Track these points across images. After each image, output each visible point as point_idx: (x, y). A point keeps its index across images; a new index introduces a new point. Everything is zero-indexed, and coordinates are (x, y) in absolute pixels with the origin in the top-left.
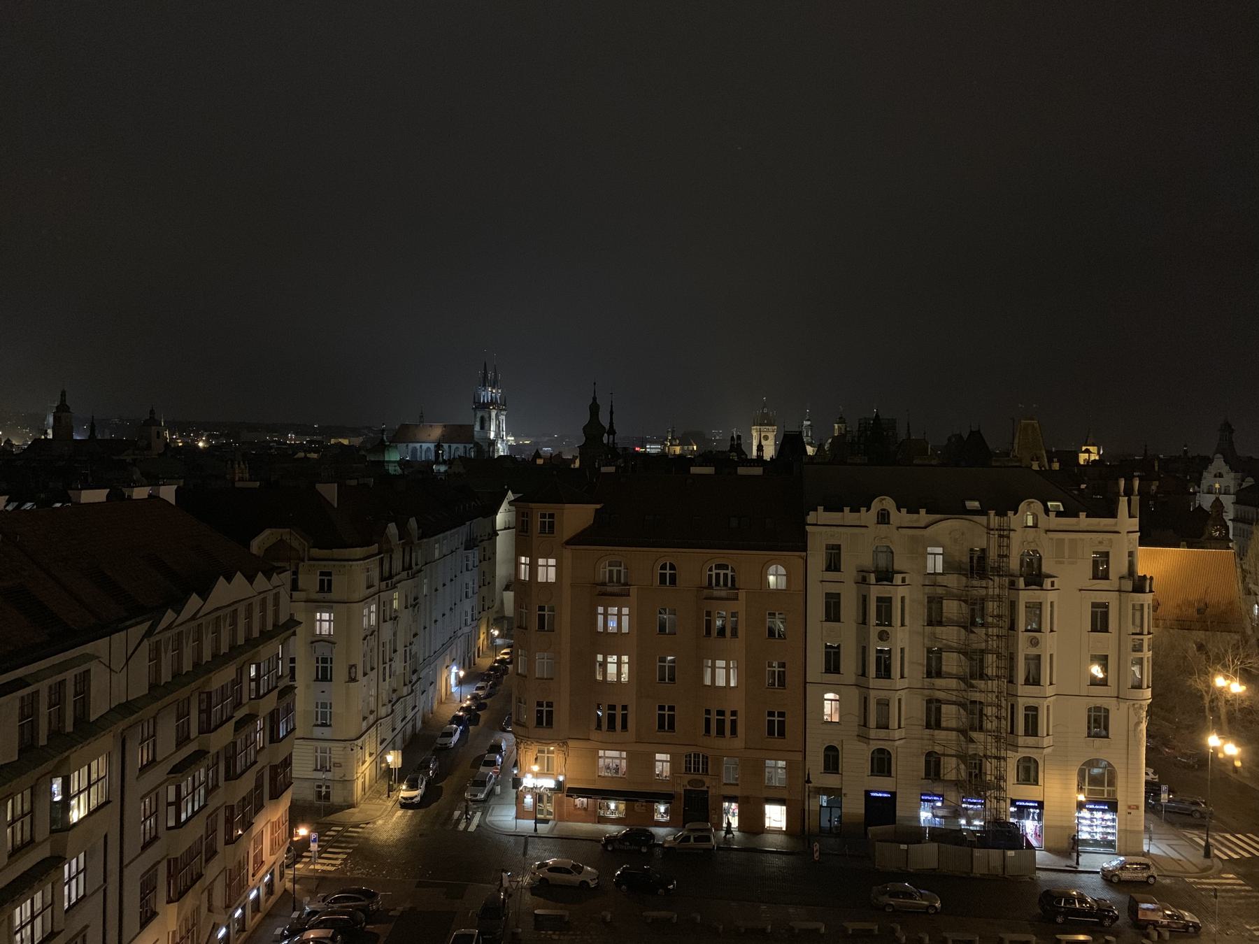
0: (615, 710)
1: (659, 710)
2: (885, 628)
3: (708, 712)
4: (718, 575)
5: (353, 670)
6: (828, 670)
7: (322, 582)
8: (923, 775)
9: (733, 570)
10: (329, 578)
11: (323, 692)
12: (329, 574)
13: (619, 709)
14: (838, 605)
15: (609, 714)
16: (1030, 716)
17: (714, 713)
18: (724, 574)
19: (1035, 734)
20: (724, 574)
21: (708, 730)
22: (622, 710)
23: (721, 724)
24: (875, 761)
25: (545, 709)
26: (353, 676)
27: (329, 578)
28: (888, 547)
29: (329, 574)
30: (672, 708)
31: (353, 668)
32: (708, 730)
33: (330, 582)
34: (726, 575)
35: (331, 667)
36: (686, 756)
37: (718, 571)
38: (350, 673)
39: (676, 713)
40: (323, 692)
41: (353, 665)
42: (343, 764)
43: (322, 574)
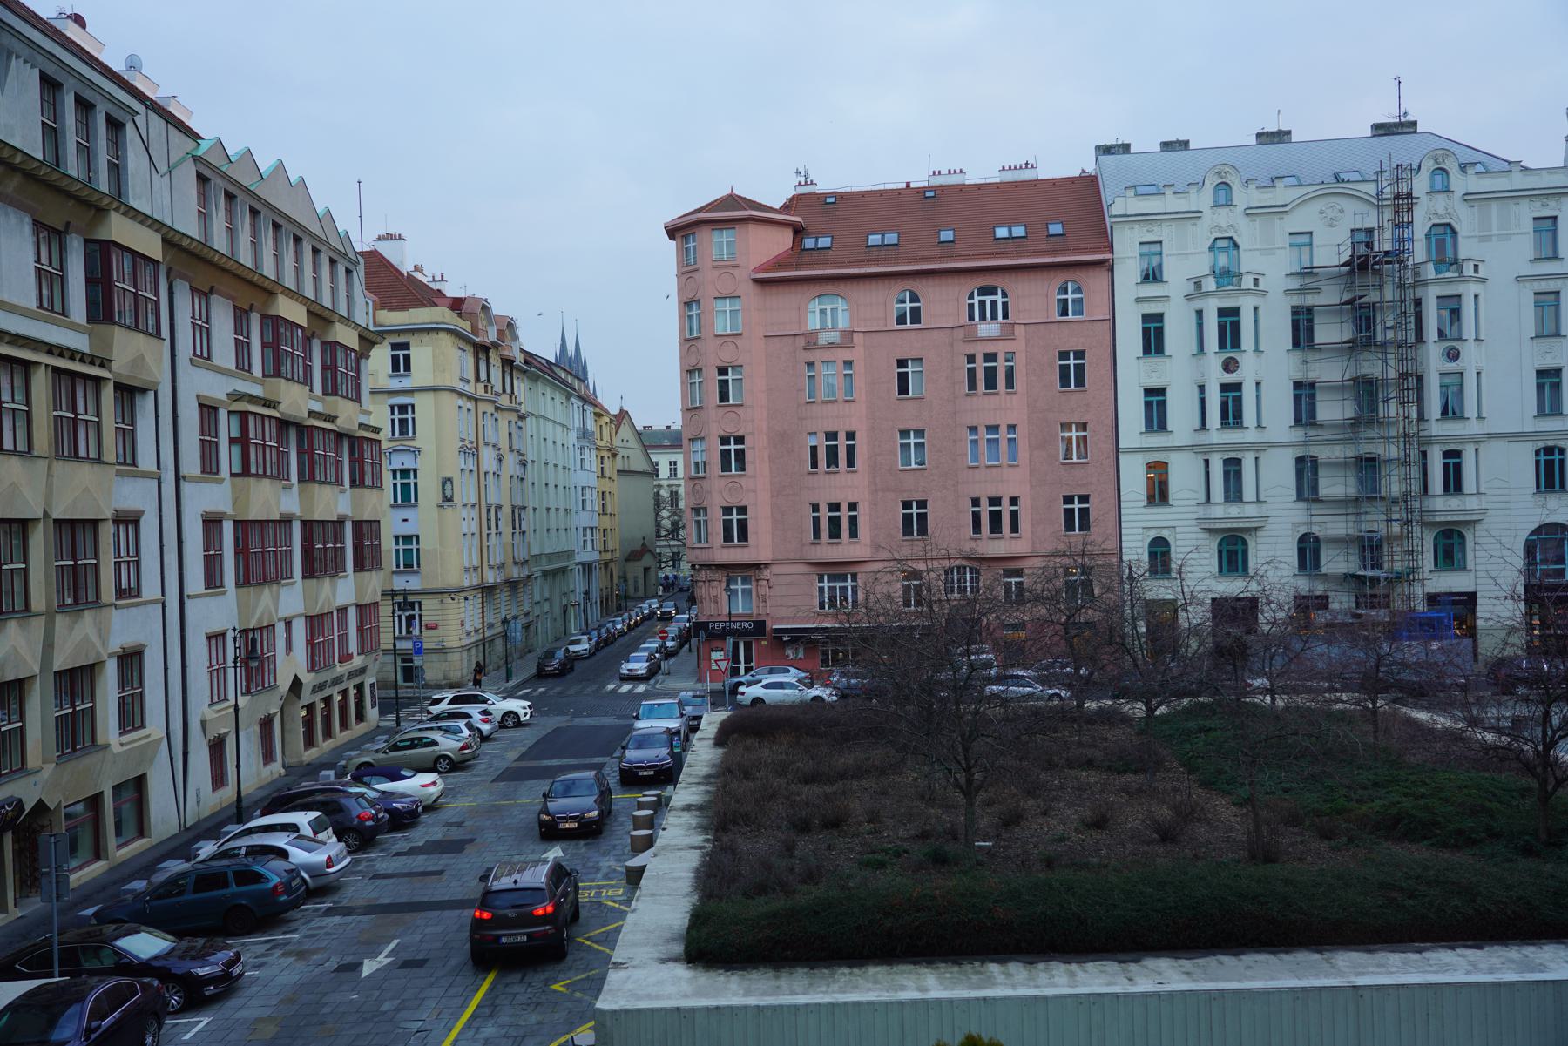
0: (838, 510)
1: (1064, 503)
2: (1454, 344)
3: (816, 508)
4: (982, 304)
5: (448, 486)
6: (1149, 427)
7: (395, 360)
8: (1215, 569)
9: (1004, 295)
10: (406, 352)
11: (405, 520)
12: (406, 346)
13: (844, 507)
14: (1160, 332)
15: (903, 514)
16: (1451, 465)
17: (984, 502)
18: (404, 355)
19: (1458, 488)
20: (404, 355)
21: (817, 534)
22: (850, 510)
23: (835, 523)
24: (1224, 555)
25: (735, 517)
26: (448, 493)
27: (406, 352)
28: (1231, 238)
29: (406, 346)
30: (922, 504)
31: (449, 483)
32: (817, 534)
33: (407, 358)
34: (994, 303)
35: (416, 484)
36: (946, 573)
37: (982, 298)
38: (444, 490)
39: (929, 510)
40: (405, 520)
41: (449, 479)
42: (440, 623)
43: (395, 346)
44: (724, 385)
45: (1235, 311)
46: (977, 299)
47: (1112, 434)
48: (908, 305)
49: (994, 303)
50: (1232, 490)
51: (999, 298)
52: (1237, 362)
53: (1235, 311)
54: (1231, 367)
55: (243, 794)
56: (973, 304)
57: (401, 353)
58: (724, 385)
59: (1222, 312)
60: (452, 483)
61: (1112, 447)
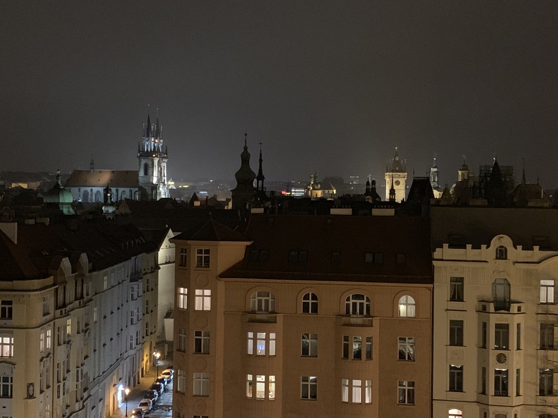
4: (354, 304)
5: (31, 388)
9: (368, 300)
10: (10, 306)
12: (10, 303)
14: (461, 330)
26: (31, 393)
27: (10, 306)
29: (10, 303)
31: (31, 386)
33: (10, 310)
34: (362, 305)
35: (12, 386)
37: (260, 298)
38: (28, 390)
41: (32, 384)
44: (198, 342)
45: (506, 327)
46: (257, 298)
47: (430, 391)
48: (310, 301)
49: (362, 305)
50: (498, 254)
51: (365, 302)
52: (506, 357)
53: (506, 327)
54: (502, 359)
55: (490, 314)
56: (255, 301)
57: (7, 307)
58: (198, 342)
59: (498, 326)
60: (33, 387)
61: (429, 398)
